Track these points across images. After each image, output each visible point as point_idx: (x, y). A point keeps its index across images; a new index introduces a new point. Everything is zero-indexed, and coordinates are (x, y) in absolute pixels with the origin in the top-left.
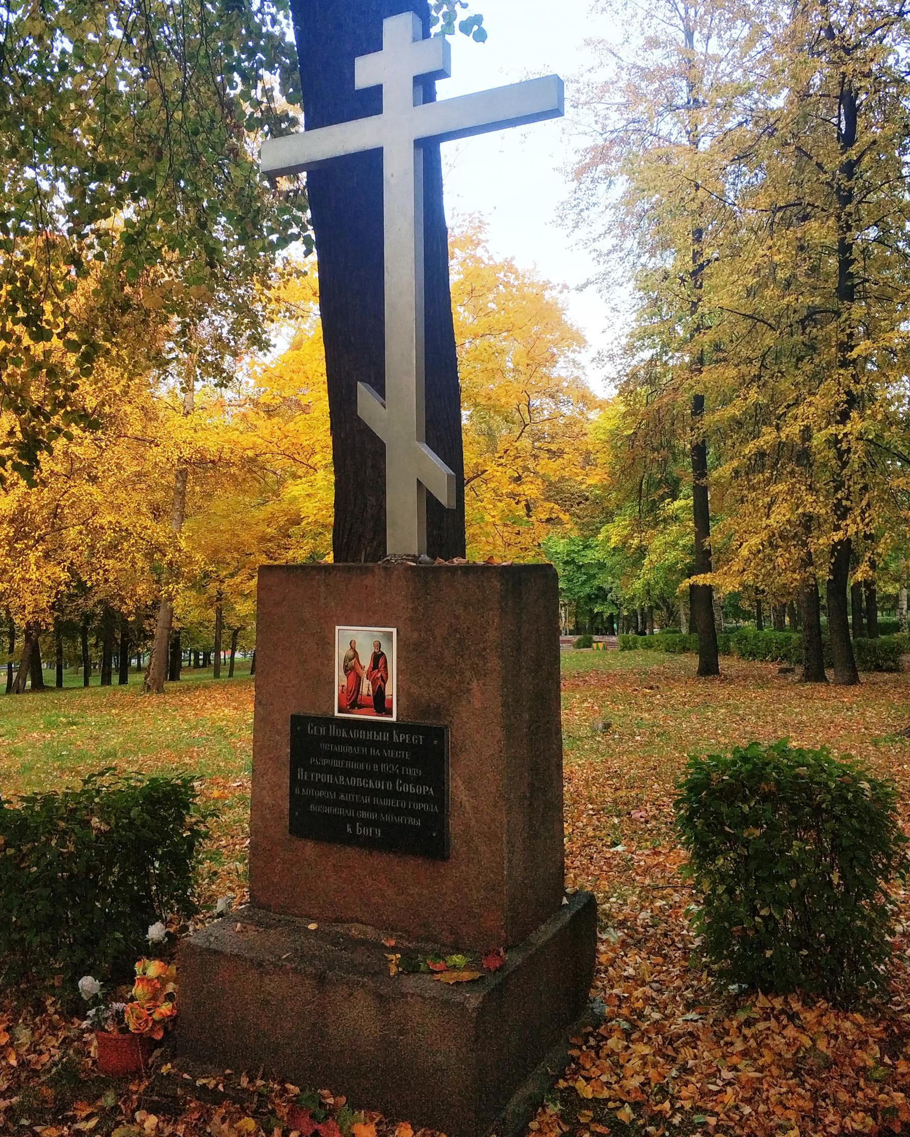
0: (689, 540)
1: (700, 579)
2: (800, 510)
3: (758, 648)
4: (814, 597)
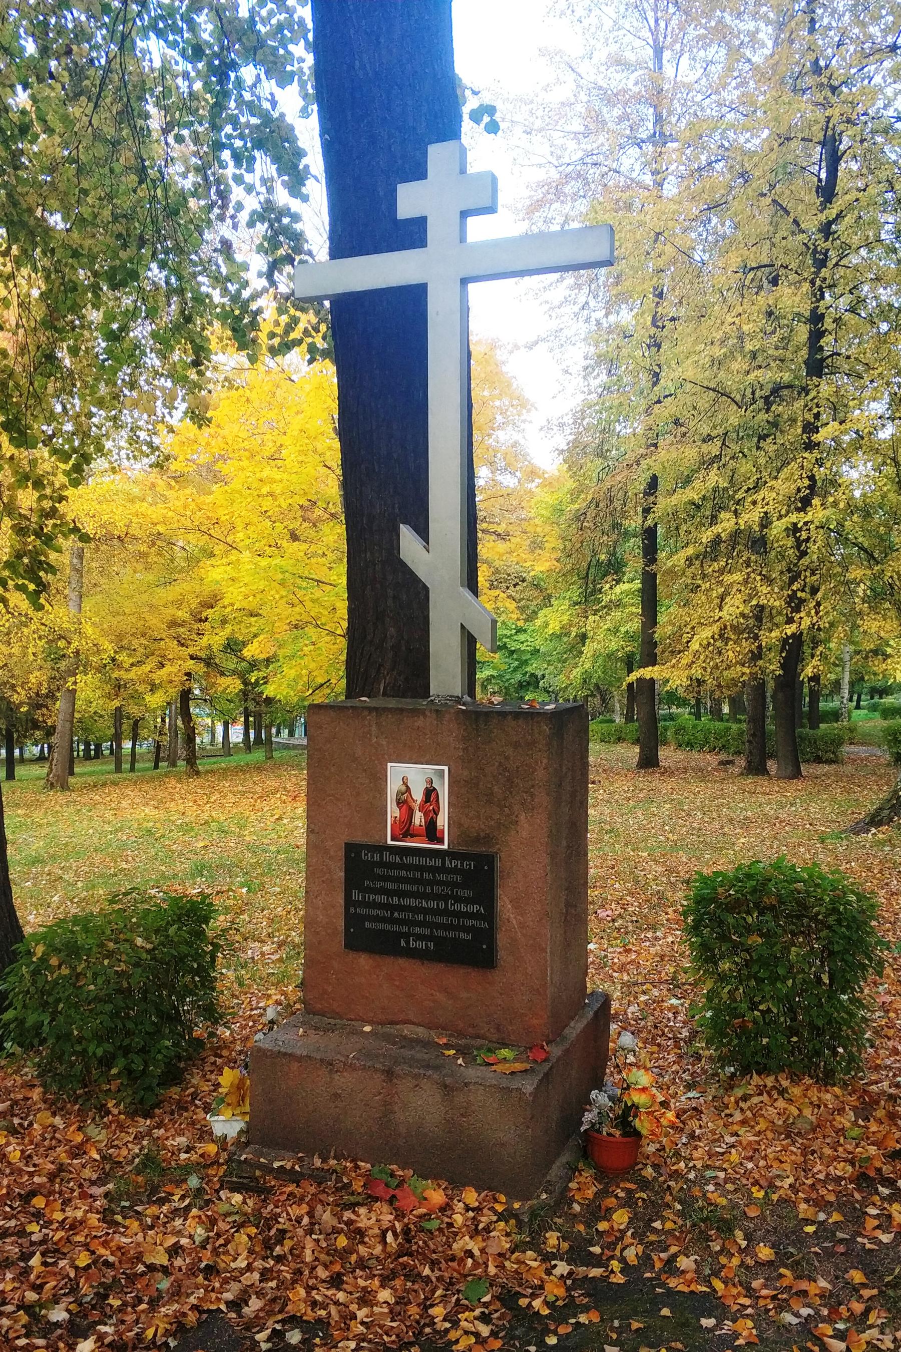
0: (635, 625)
1: (647, 673)
2: (754, 602)
3: (696, 738)
4: (761, 687)
